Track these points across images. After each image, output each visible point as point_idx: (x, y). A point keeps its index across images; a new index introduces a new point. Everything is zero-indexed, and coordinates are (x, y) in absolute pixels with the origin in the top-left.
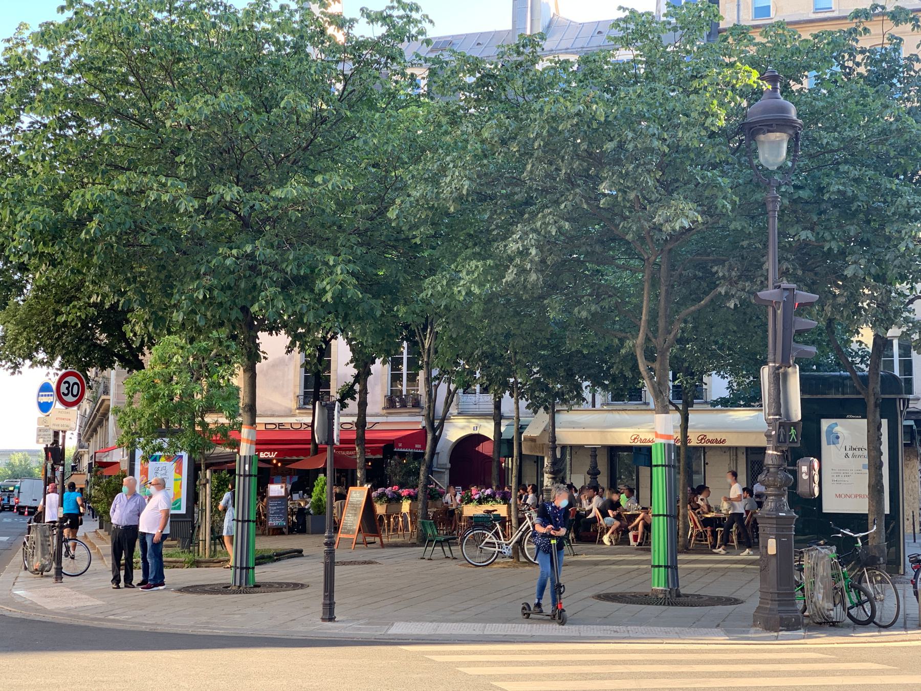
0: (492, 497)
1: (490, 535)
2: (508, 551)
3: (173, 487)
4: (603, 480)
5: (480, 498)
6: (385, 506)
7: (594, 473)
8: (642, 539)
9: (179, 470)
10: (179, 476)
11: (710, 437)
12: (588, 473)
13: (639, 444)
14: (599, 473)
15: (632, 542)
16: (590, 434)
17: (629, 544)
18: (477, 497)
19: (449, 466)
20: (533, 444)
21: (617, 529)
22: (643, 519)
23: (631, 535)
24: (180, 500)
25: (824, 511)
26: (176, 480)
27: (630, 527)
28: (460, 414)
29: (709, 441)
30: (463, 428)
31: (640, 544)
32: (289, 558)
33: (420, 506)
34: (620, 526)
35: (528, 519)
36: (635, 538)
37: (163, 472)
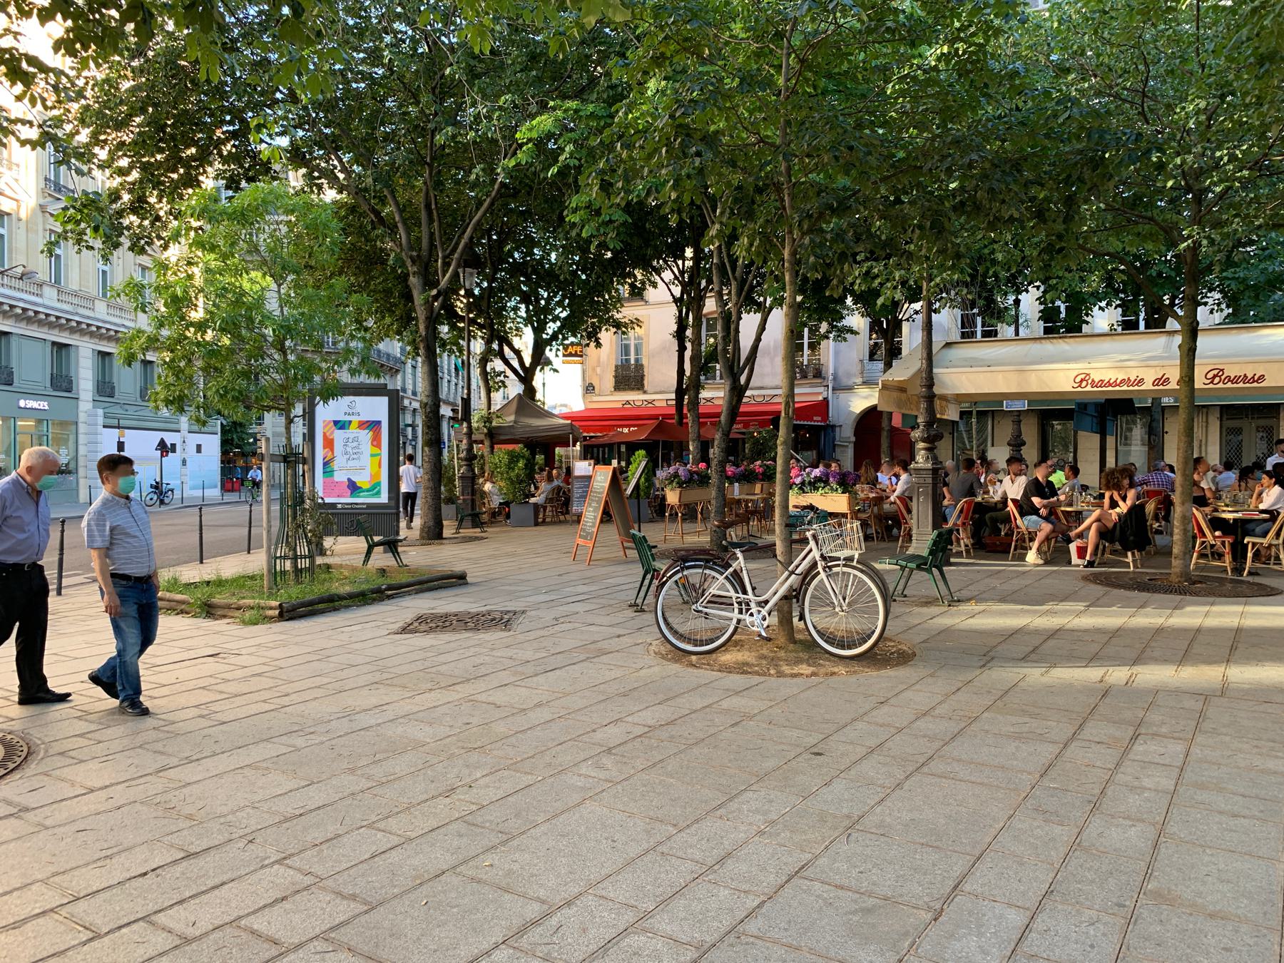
0: (821, 482)
1: (721, 578)
2: (758, 621)
3: (369, 465)
4: (1030, 453)
5: (803, 483)
6: (678, 491)
7: (1017, 444)
8: (1095, 553)
9: (376, 441)
10: (376, 451)
11: (1232, 371)
12: (1009, 444)
13: (1089, 388)
14: (1024, 444)
15: (1075, 559)
16: (1000, 376)
17: (1069, 563)
18: (798, 480)
19: (853, 439)
20: (903, 396)
21: (1047, 539)
22: (1098, 520)
23: (1073, 547)
24: (379, 484)
25: (386, 399)
26: (372, 455)
27: (1072, 534)
28: (864, 383)
29: (1229, 379)
30: (866, 398)
31: (1091, 564)
32: (417, 592)
33: (714, 493)
34: (1053, 531)
35: (812, 544)
36: (1082, 552)
37: (355, 444)
